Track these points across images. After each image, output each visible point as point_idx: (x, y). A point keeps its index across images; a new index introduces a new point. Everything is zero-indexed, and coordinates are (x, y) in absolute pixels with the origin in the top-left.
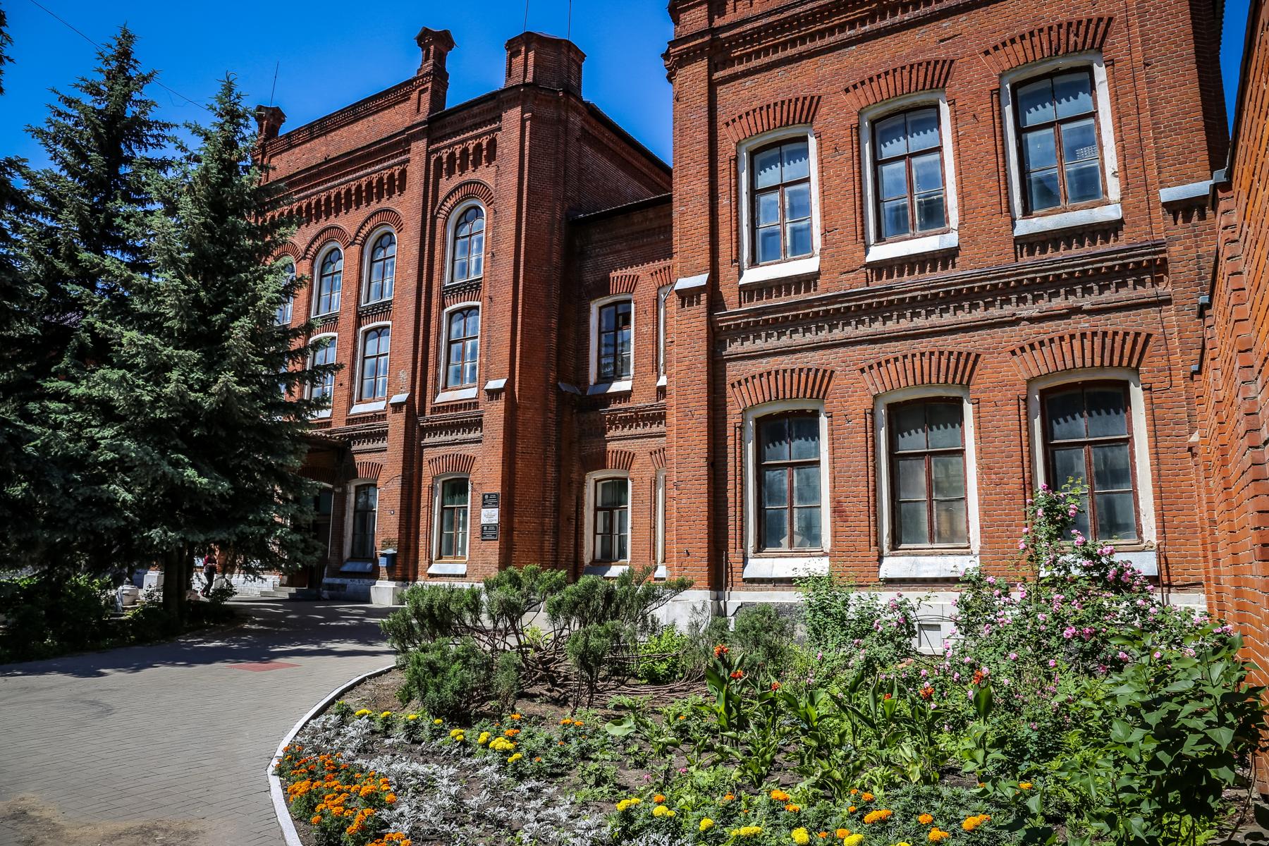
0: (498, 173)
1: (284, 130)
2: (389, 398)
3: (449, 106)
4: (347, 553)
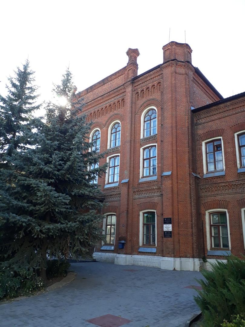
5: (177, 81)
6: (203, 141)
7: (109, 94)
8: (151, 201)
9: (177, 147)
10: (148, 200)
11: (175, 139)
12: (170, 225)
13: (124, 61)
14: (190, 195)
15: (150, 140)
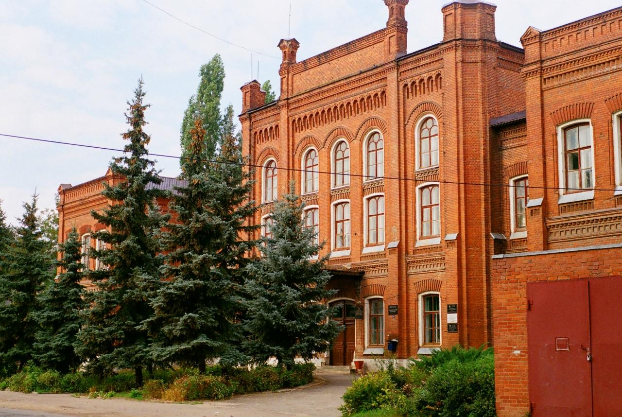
2: (387, 244)
3: (410, 50)
10: (429, 276)
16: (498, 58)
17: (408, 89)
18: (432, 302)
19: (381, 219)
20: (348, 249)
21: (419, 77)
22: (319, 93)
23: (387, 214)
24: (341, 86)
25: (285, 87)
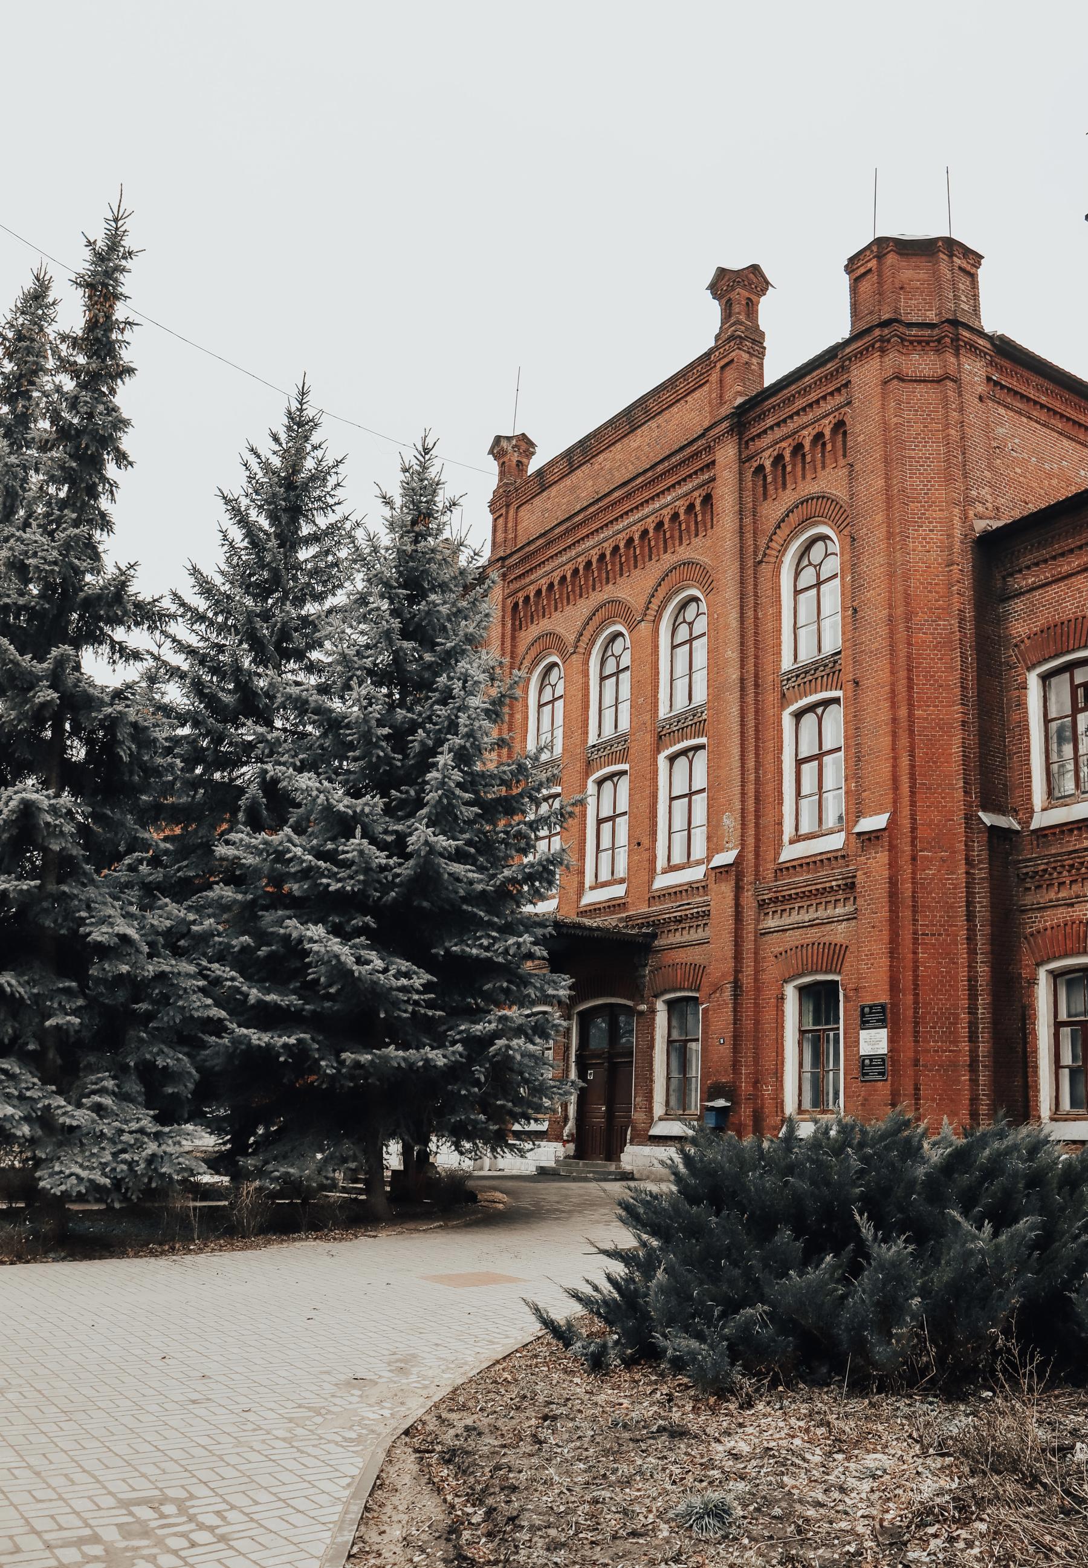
0: (852, 477)
1: (534, 465)
4: (659, 1109)
5: (908, 415)
6: (1029, 669)
7: (650, 474)
8: (823, 940)
9: (911, 707)
10: (813, 935)
11: (902, 674)
12: (883, 1034)
13: (701, 326)
14: (967, 906)
15: (819, 674)
16: (989, 379)
17: (761, 480)
18: (821, 999)
19: (700, 803)
20: (622, 881)
21: (790, 440)
22: (567, 531)
23: (713, 789)
24: (614, 504)
25: (500, 536)
